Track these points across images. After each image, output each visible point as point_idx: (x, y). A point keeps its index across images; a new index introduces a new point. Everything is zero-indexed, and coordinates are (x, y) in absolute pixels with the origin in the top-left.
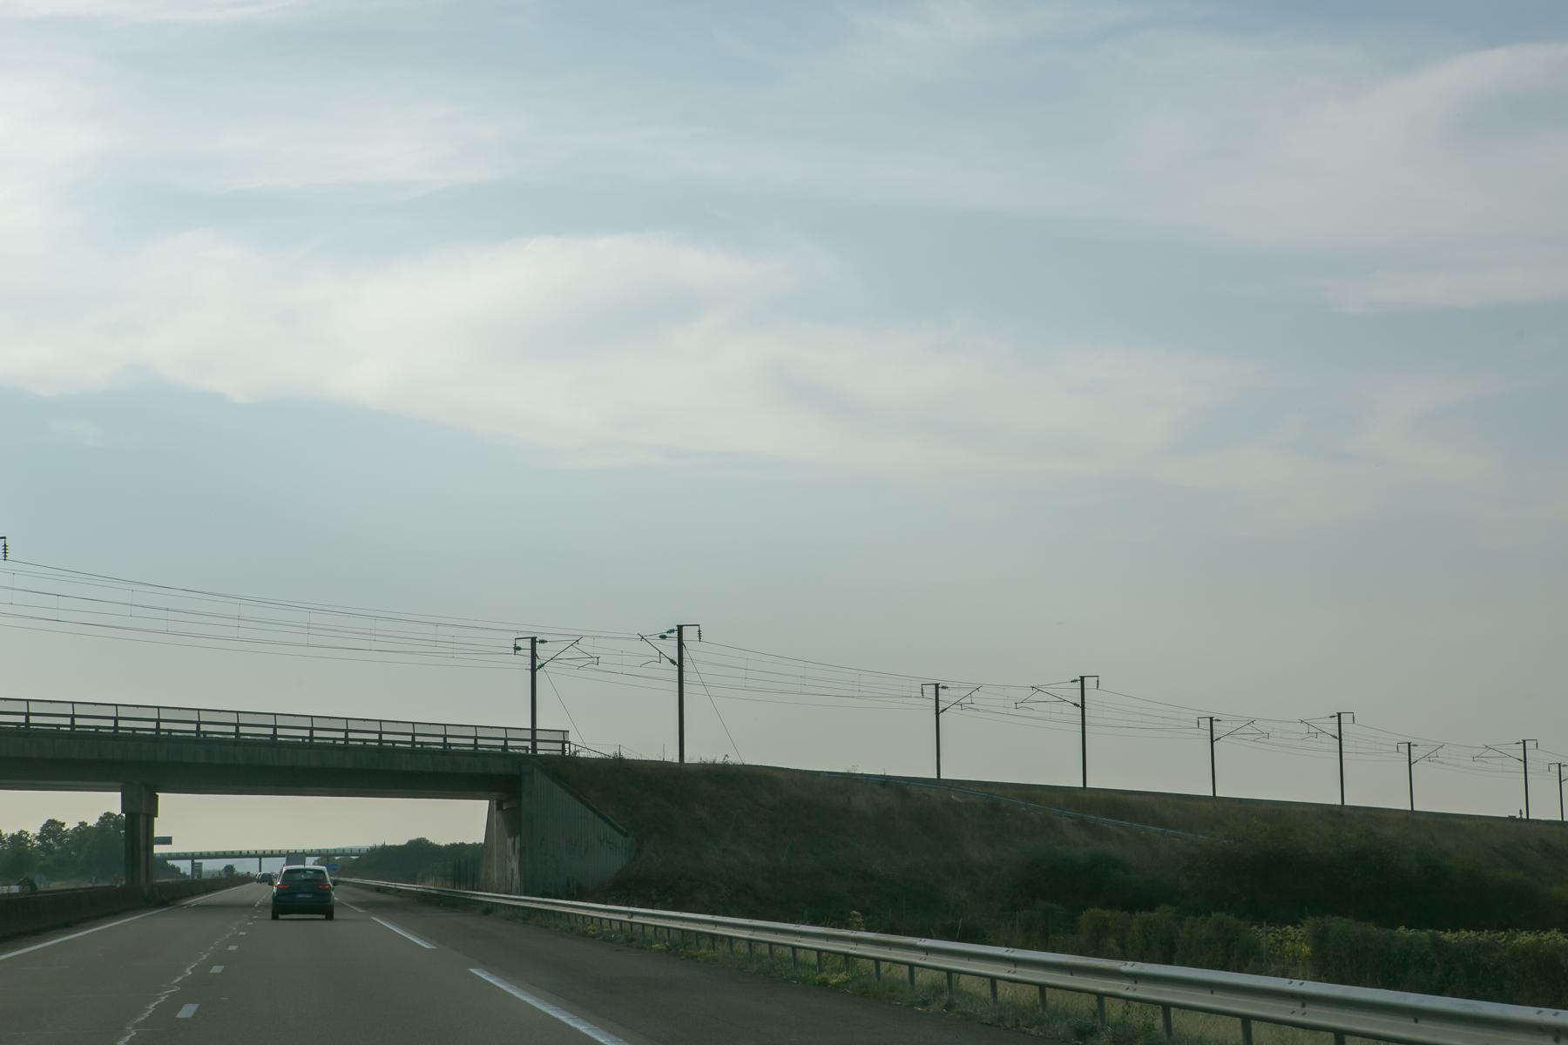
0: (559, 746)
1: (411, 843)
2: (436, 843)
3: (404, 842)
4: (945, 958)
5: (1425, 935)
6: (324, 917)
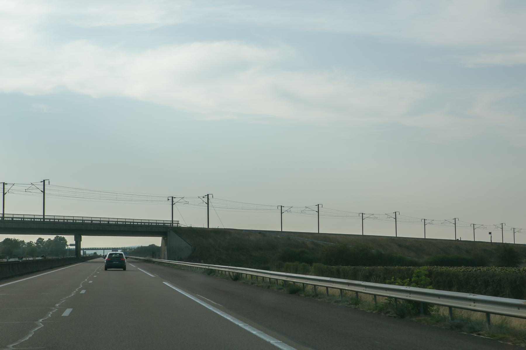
0: (177, 225)
1: (150, 246)
2: (158, 246)
3: (147, 245)
4: (402, 294)
5: (326, 266)
6: (123, 269)
